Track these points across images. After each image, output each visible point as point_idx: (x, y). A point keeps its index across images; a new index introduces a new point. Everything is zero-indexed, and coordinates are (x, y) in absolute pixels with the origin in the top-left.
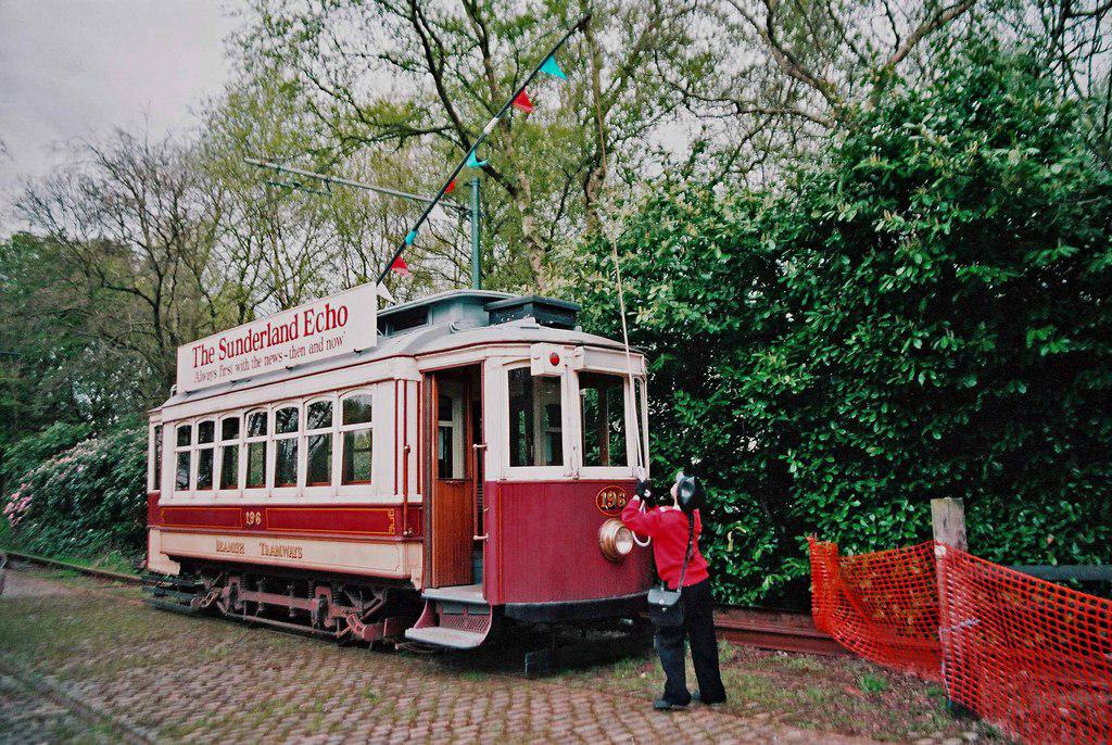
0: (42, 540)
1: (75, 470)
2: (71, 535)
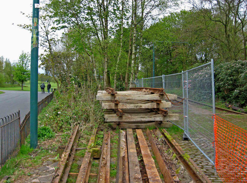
0: (196, 96)
1: (205, 76)
2: (205, 95)
